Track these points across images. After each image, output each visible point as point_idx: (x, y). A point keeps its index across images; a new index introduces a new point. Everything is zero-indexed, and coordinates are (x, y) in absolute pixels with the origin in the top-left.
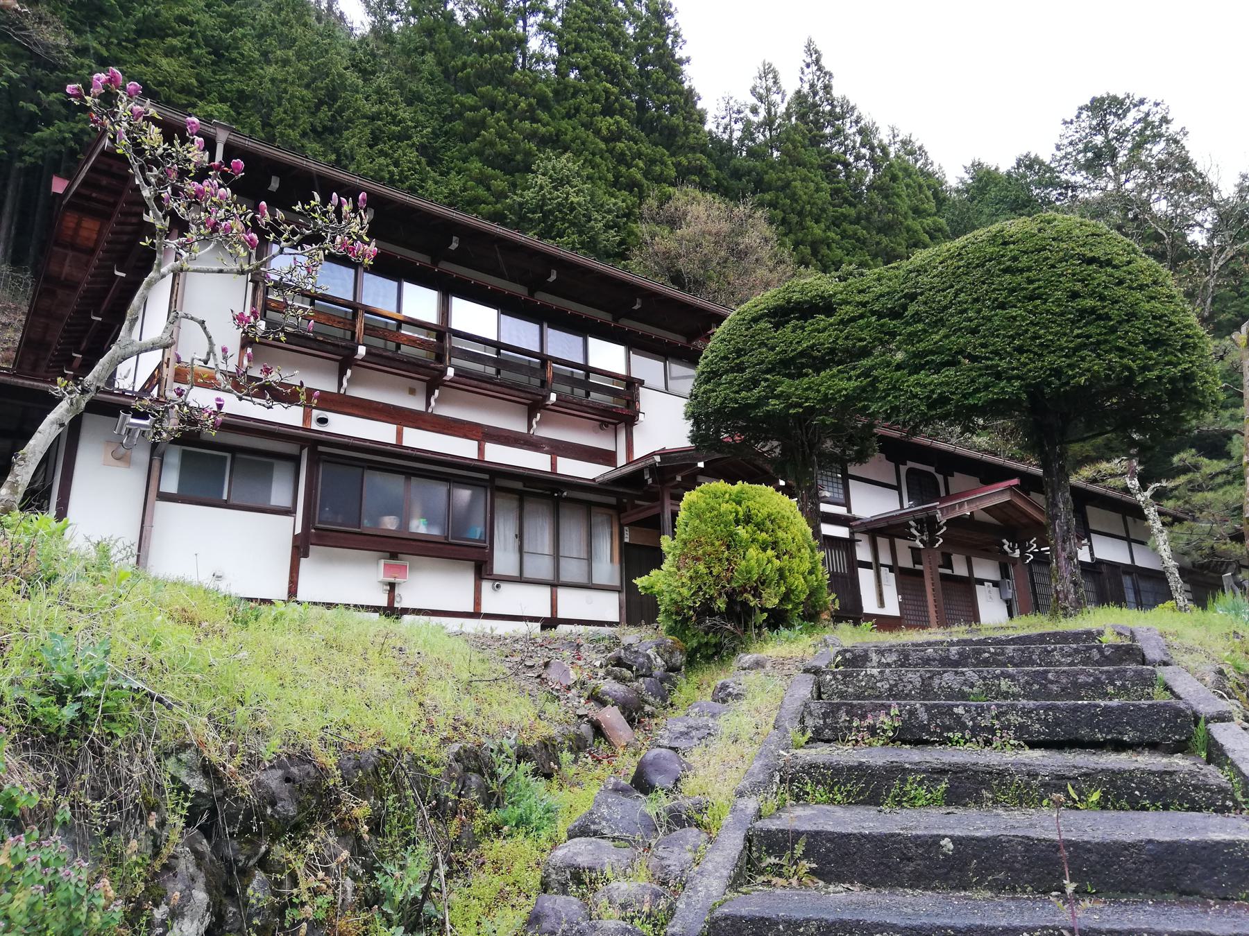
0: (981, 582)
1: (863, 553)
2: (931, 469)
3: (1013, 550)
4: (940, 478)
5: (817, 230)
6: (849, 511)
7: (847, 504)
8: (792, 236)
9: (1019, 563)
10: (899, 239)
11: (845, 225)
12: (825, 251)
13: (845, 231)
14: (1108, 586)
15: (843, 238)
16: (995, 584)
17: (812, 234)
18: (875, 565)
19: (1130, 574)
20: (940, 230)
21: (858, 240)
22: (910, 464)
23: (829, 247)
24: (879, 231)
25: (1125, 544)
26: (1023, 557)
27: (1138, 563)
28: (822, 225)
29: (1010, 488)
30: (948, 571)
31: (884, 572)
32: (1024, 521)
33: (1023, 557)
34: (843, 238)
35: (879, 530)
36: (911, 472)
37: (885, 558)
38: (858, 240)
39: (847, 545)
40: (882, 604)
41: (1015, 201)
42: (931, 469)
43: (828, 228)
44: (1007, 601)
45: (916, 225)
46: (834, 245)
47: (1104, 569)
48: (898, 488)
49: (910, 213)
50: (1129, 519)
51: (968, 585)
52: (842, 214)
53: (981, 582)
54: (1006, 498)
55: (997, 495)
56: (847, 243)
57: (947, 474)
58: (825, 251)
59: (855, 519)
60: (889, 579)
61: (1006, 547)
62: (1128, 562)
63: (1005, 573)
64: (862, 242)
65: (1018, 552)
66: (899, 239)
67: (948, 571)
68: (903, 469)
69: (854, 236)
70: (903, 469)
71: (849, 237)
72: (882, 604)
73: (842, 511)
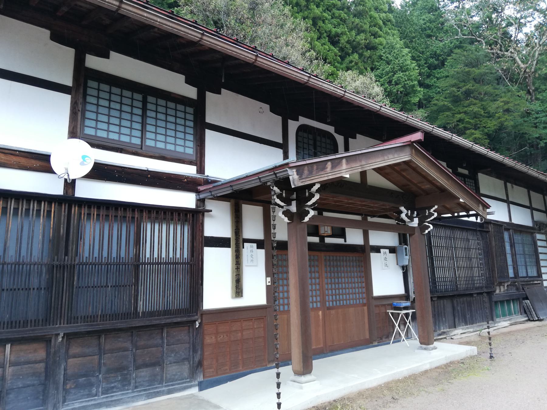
0: (377, 249)
1: (217, 224)
2: (330, 129)
3: (411, 218)
4: (340, 139)
5: (317, 11)
6: (201, 170)
7: (199, 162)
8: (301, 14)
9: (417, 233)
10: (365, 21)
11: (334, 11)
12: (320, 23)
13: (334, 14)
14: (494, 244)
15: (332, 18)
16: (392, 250)
17: (314, 13)
18: (236, 242)
19: (507, 230)
20: (389, 21)
21: (341, 20)
22: (303, 120)
23: (324, 22)
24: (355, 16)
25: (505, 205)
26: (422, 227)
27: (515, 221)
28: (321, 9)
29: (411, 145)
30: (340, 241)
31: (249, 250)
32: (427, 186)
33: (422, 227)
34: (332, 18)
35: (241, 195)
36: (302, 129)
37: (253, 229)
38: (341, 20)
39: (193, 218)
40: (238, 291)
41: (431, 8)
42: (330, 129)
43: (324, 11)
44: (403, 267)
45: (376, 15)
46: (327, 21)
47: (491, 228)
48: (283, 146)
49: (373, 9)
50: (509, 185)
51: (363, 253)
52: (333, 4)
53: (377, 249)
54: (404, 157)
55: (396, 153)
56: (334, 21)
57: (349, 135)
58: (320, 23)
59: (207, 182)
60: (255, 262)
61: (403, 216)
62: (507, 220)
63: (403, 240)
64: (344, 21)
65: (416, 220)
66: (365, 21)
67: (340, 241)
68: (293, 126)
69: (339, 17)
70: (293, 126)
71: (336, 18)
72: (238, 291)
73: (190, 170)
